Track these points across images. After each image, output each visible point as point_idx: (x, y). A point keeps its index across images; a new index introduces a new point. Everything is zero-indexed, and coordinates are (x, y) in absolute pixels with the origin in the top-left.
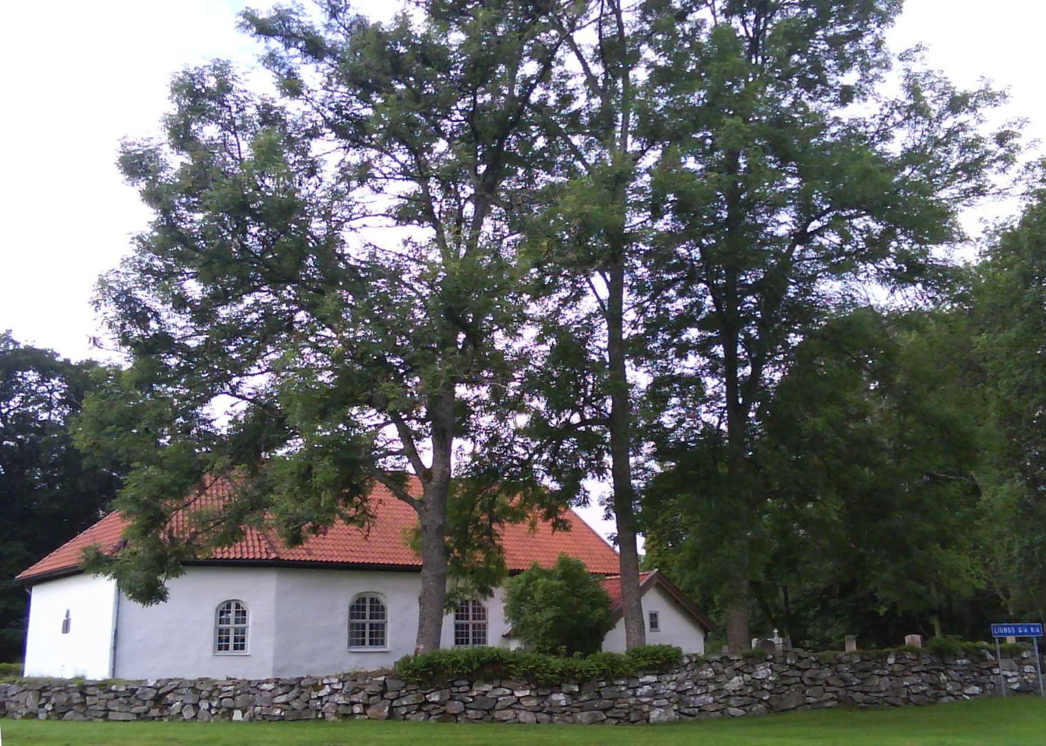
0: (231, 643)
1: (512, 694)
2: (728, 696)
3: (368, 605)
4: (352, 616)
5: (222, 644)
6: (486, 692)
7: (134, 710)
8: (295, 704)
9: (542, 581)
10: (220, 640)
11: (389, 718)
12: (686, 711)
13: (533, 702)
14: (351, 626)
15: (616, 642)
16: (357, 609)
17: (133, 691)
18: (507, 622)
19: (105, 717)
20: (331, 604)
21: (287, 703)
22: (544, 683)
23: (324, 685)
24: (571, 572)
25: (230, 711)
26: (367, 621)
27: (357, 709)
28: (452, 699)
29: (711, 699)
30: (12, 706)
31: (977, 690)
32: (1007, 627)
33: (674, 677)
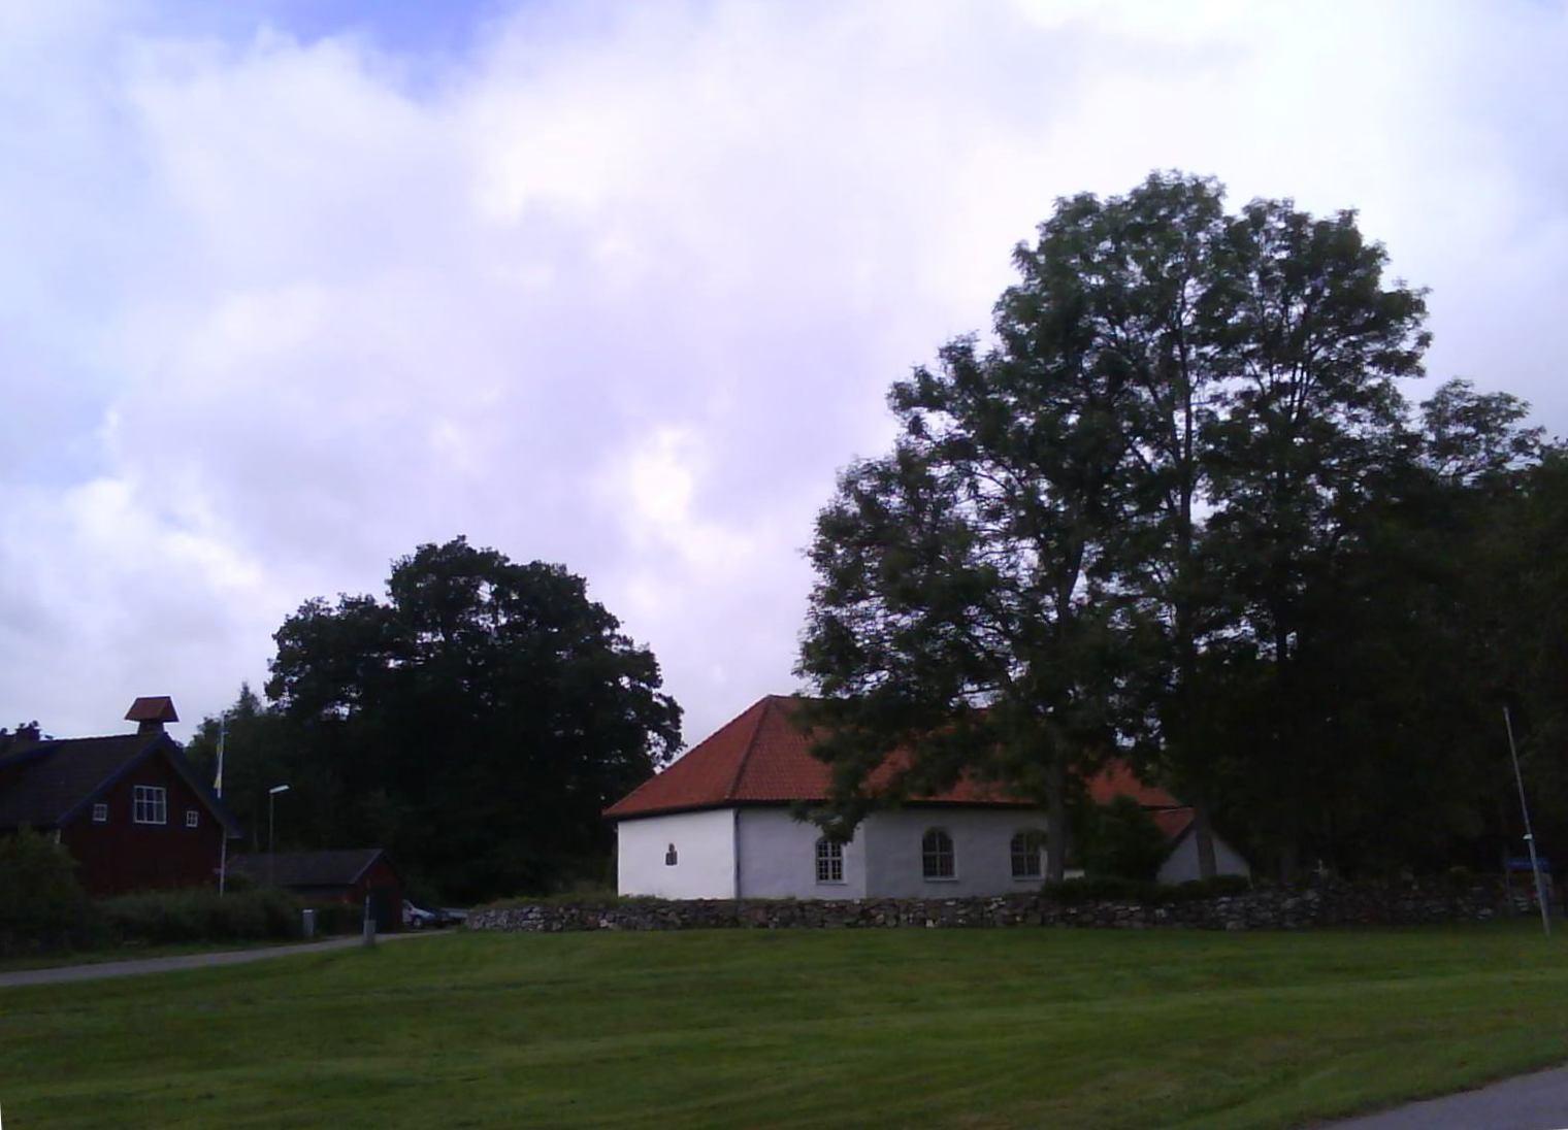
0: (830, 874)
1: (1127, 909)
5: (930, 868)
7: (846, 921)
8: (972, 915)
10: (821, 870)
14: (925, 858)
16: (928, 844)
17: (843, 908)
19: (822, 926)
20: (906, 841)
21: (966, 915)
23: (991, 903)
27: (1018, 919)
29: (1271, 915)
31: (1489, 911)
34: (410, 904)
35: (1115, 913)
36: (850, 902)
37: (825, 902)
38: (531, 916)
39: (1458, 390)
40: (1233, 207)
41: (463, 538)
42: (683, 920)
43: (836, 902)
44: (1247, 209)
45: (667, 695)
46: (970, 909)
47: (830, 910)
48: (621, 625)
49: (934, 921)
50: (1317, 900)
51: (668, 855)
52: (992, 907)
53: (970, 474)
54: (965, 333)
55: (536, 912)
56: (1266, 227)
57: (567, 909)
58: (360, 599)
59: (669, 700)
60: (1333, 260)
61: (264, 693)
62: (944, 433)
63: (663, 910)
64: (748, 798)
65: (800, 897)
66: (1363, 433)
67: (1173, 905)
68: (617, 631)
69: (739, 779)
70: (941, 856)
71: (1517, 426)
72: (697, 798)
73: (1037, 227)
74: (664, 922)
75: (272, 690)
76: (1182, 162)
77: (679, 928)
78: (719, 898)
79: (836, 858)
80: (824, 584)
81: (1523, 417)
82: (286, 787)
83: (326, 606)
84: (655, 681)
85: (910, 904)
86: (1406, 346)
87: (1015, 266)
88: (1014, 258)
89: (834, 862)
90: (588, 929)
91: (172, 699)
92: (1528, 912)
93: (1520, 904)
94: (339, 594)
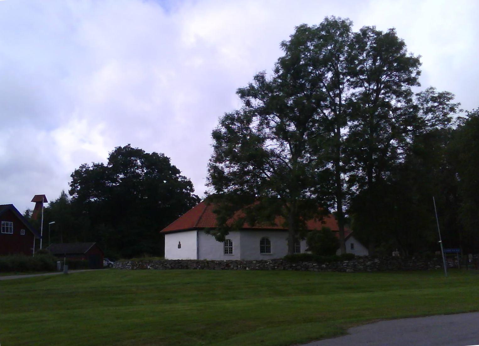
3: (265, 240)
4: (261, 244)
5: (226, 252)
6: (306, 264)
7: (221, 267)
8: (261, 266)
10: (225, 250)
13: (318, 267)
14: (261, 247)
15: (339, 253)
16: (262, 242)
17: (221, 263)
18: (307, 246)
19: (214, 269)
20: (255, 242)
24: (326, 231)
25: (245, 268)
26: (228, 246)
29: (362, 267)
31: (439, 267)
33: (352, 261)
36: (223, 261)
37: (215, 261)
38: (128, 264)
40: (356, 29)
41: (130, 145)
42: (171, 266)
44: (361, 30)
45: (196, 195)
49: (249, 268)
50: (379, 262)
51: (178, 245)
53: (266, 119)
54: (261, 71)
55: (130, 263)
56: (368, 35)
60: (388, 47)
62: (257, 105)
63: (166, 263)
64: (201, 227)
65: (208, 259)
67: (328, 264)
69: (199, 220)
70: (264, 244)
71: (451, 102)
72: (186, 227)
73: (290, 36)
74: (165, 267)
75: (71, 193)
77: (170, 269)
78: (192, 259)
79: (231, 247)
80: (214, 155)
81: (453, 99)
82: (54, 222)
83: (88, 166)
84: (192, 190)
85: (241, 262)
86: (413, 75)
87: (281, 49)
88: (281, 46)
92: (452, 267)
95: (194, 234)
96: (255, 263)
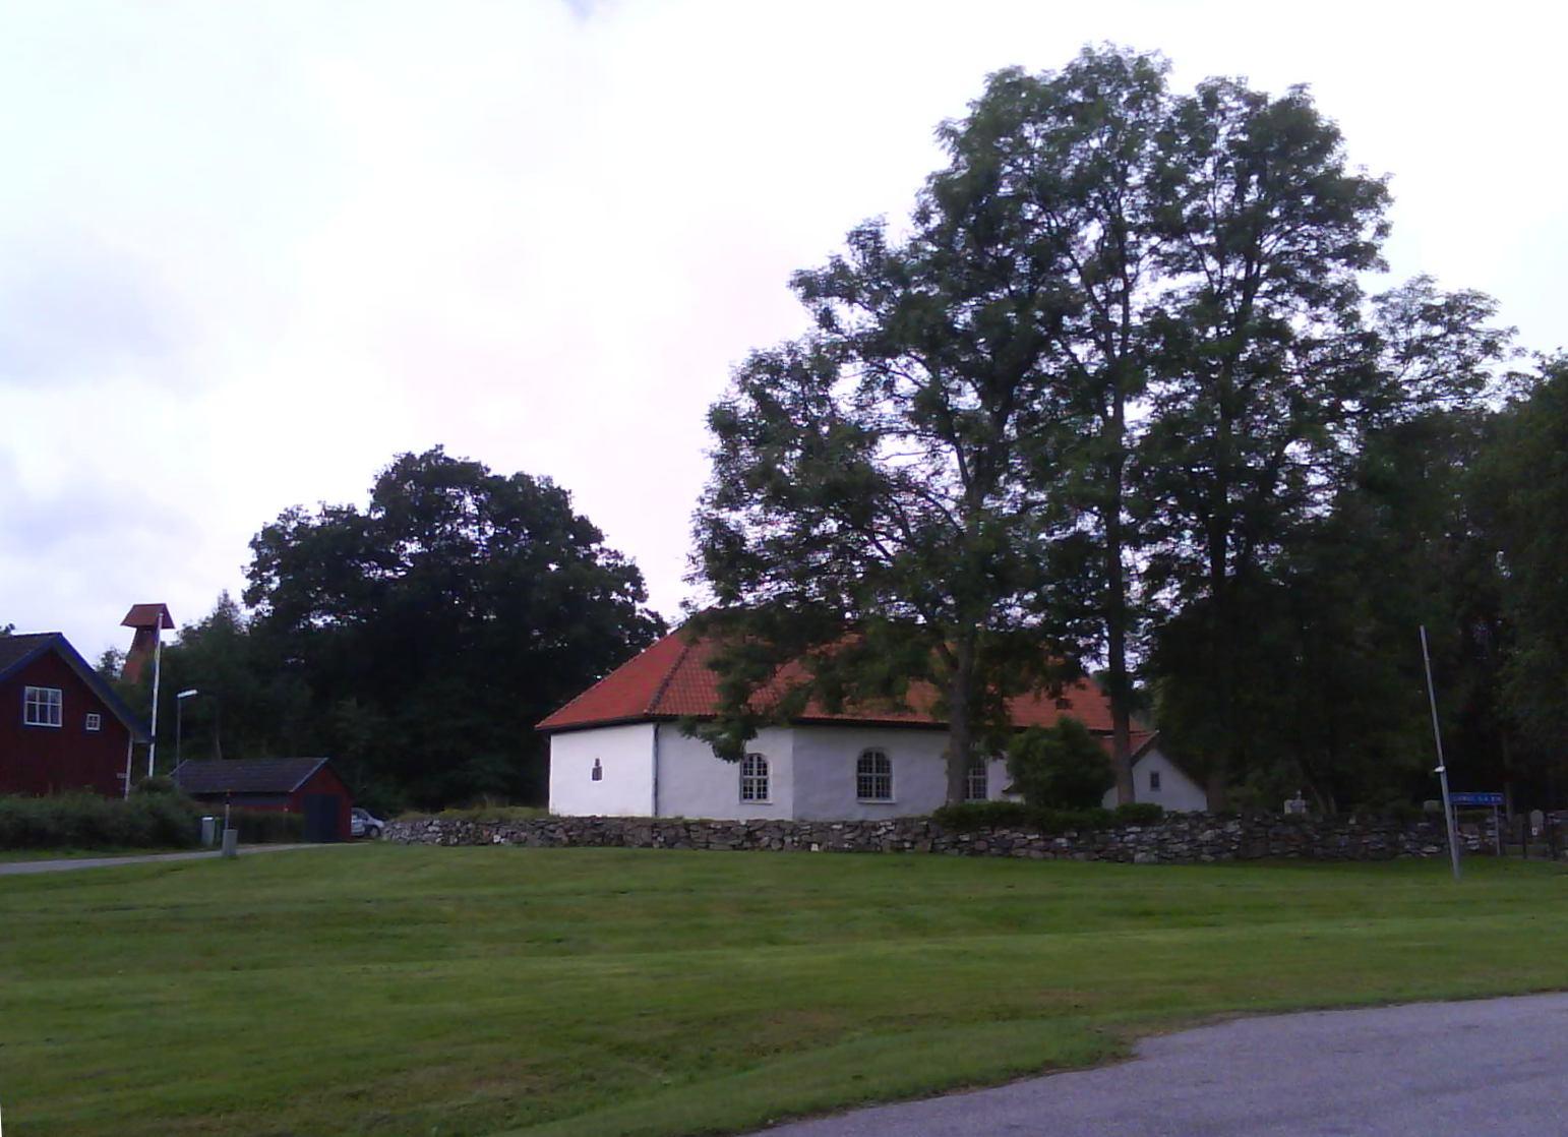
2: (1201, 846)
5: (864, 791)
7: (731, 843)
8: (860, 840)
9: (1045, 742)
10: (745, 789)
11: (931, 852)
12: (1165, 855)
14: (860, 779)
15: (1111, 801)
16: (864, 764)
17: (730, 828)
19: (707, 847)
20: (841, 761)
21: (853, 840)
22: (1049, 830)
23: (880, 827)
24: (1070, 733)
25: (809, 845)
27: (907, 845)
28: (979, 840)
29: (1185, 847)
30: (629, 838)
31: (1435, 849)
32: (1463, 801)
33: (1155, 829)
34: (366, 813)
35: (1013, 841)
36: (736, 823)
37: (711, 821)
38: (430, 829)
39: (1424, 286)
40: (1180, 85)
41: (441, 447)
42: (570, 837)
43: (722, 822)
44: (1201, 88)
45: (653, 610)
46: (859, 832)
47: (716, 831)
48: (606, 538)
49: (819, 845)
50: (1239, 833)
52: (879, 833)
53: (885, 370)
55: (436, 825)
57: (464, 823)
58: (342, 507)
59: (655, 615)
60: (1285, 149)
61: (242, 600)
63: (551, 827)
66: (1325, 334)
68: (604, 544)
71: (1487, 324)
74: (551, 839)
75: (251, 598)
76: (1130, 39)
77: (566, 846)
80: (714, 486)
81: (1493, 315)
82: (194, 692)
83: (305, 514)
84: (641, 596)
86: (1365, 236)
89: (759, 782)
90: (483, 844)
91: (137, 603)
93: (1469, 842)
94: (319, 502)
95: (646, 733)
96: (840, 830)
